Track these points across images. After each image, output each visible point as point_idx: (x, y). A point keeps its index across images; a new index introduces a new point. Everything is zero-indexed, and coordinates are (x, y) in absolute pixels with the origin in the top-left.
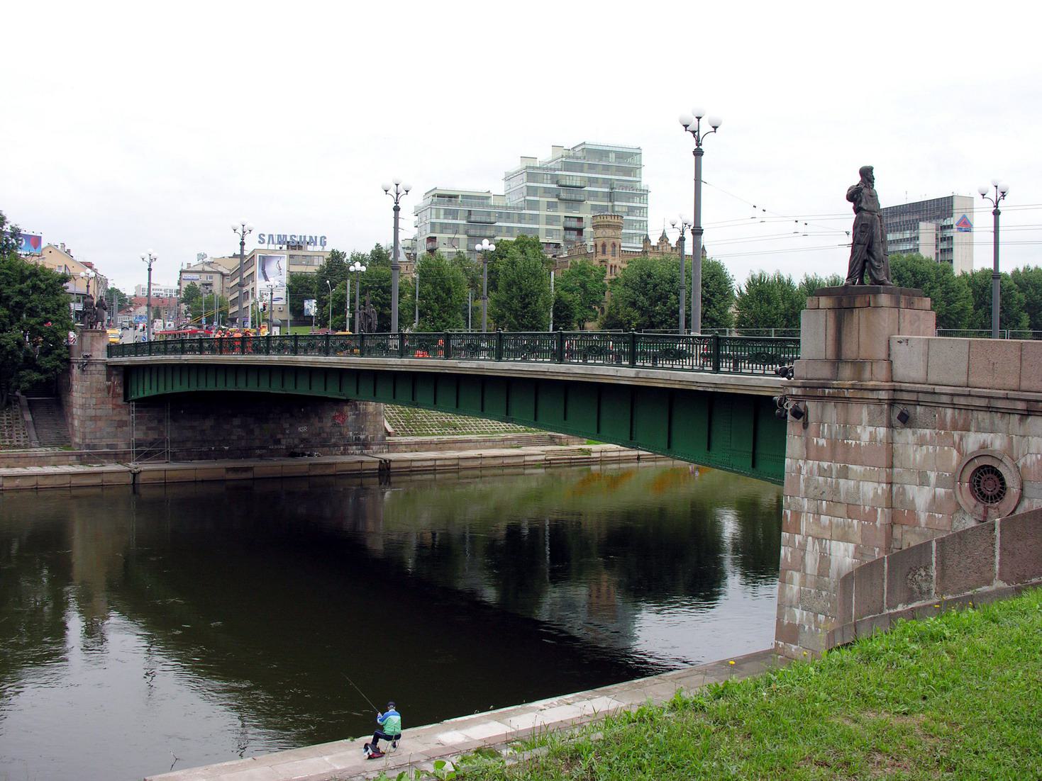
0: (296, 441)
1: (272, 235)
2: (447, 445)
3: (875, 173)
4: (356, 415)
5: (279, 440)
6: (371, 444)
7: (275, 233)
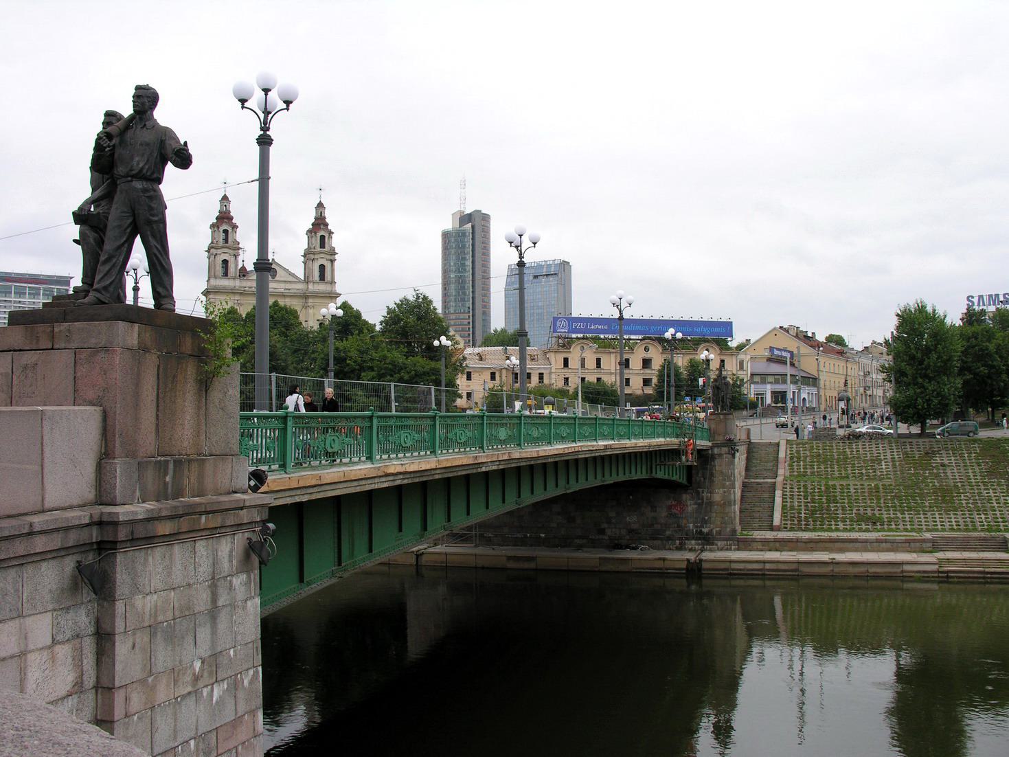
0: (624, 532)
1: (998, 295)
2: (838, 545)
3: (350, 302)
4: (699, 504)
5: (604, 529)
6: (714, 539)
7: (985, 293)
